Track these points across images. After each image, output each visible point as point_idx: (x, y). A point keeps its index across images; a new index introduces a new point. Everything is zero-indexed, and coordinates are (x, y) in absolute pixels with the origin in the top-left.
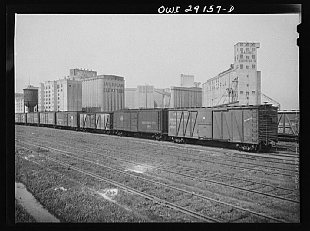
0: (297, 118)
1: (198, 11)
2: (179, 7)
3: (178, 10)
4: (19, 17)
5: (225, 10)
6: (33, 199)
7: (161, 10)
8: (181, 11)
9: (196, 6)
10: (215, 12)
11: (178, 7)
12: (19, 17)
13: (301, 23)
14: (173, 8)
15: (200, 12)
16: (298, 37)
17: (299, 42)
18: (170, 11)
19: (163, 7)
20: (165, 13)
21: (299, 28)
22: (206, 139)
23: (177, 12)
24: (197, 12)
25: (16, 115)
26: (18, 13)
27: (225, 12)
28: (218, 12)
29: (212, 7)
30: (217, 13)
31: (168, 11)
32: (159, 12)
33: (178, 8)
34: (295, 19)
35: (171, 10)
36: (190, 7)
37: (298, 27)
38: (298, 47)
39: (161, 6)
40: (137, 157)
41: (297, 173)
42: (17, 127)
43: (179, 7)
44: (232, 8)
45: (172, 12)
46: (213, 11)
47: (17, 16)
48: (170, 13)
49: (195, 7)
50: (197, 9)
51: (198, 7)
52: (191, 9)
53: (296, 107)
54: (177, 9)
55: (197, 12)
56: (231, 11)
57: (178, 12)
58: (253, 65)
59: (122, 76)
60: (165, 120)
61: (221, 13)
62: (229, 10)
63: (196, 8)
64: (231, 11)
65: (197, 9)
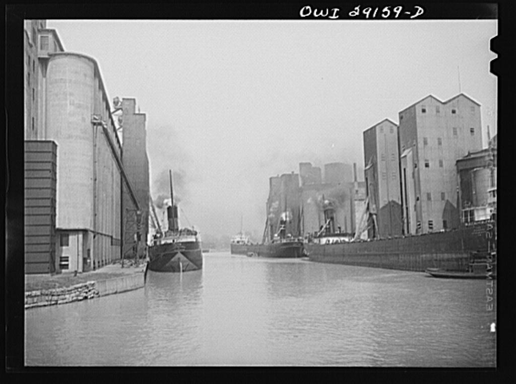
1: (369, 16)
2: (338, 10)
8: (343, 16)
9: (396, 7)
10: (392, 17)
11: (336, 10)
13: (497, 35)
17: (495, 67)
19: (308, 7)
21: (495, 45)
22: (479, 223)
24: (367, 17)
27: (408, 17)
28: (397, 16)
29: (389, 9)
32: (302, 15)
33: (337, 11)
34: (489, 28)
35: (324, 13)
38: (495, 78)
39: (307, 6)
42: (28, 277)
43: (338, 10)
44: (352, 14)
48: (320, 18)
49: (363, 9)
50: (398, 11)
51: (401, 8)
52: (334, 11)
55: (367, 17)
56: (417, 14)
58: (68, 257)
60: (417, 186)
61: (400, 18)
62: (415, 14)
63: (367, 11)
64: (417, 14)
65: (398, 11)
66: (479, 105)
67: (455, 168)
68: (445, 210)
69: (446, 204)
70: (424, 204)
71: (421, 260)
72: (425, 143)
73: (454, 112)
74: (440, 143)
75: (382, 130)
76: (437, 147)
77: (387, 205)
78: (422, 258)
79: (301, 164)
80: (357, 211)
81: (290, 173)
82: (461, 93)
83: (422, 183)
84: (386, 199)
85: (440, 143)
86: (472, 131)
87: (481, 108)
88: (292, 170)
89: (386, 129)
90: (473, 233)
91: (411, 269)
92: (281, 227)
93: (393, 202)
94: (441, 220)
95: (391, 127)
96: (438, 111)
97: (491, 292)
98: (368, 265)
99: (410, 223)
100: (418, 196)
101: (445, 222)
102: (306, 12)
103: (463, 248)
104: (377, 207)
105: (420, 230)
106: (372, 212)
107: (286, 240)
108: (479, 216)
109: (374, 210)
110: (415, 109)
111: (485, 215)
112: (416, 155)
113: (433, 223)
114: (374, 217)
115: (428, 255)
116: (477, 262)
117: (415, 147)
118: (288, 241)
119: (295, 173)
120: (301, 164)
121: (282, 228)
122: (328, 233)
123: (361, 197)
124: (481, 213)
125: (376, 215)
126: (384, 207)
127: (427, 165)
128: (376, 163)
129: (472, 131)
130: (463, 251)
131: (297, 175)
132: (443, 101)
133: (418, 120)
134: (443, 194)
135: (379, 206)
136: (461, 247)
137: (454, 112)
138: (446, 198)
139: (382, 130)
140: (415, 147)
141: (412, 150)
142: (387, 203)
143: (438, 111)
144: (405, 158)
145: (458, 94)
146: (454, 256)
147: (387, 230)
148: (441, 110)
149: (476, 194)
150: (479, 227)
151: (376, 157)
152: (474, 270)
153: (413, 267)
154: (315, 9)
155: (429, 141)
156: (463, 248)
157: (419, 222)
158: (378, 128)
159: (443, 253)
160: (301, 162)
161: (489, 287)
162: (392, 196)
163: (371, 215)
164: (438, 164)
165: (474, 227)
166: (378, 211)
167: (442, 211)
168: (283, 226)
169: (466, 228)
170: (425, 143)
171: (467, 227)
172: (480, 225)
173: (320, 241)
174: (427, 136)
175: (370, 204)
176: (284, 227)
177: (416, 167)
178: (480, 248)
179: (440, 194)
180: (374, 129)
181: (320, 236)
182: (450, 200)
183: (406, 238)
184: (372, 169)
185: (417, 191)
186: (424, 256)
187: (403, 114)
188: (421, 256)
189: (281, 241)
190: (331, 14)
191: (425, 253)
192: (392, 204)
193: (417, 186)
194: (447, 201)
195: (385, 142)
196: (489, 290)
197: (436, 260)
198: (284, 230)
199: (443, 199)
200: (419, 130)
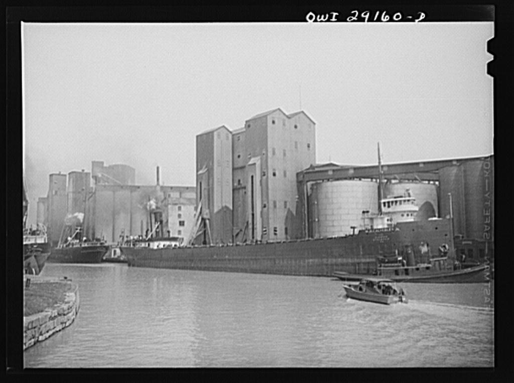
0: (491, 165)
2: (337, 14)
3: (336, 18)
4: (27, 29)
5: (410, 17)
6: (129, 269)
7: (311, 17)
11: (335, 14)
12: (27, 29)
14: (327, 16)
15: (371, 20)
16: (492, 36)
17: (492, 69)
18: (322, 19)
19: (311, 13)
20: (316, 21)
21: (492, 46)
23: (334, 19)
24: (366, 20)
25: (494, 19)
26: (25, 21)
30: (347, 21)
31: (320, 18)
33: (336, 16)
34: (485, 30)
35: (325, 18)
36: (355, 13)
37: (489, 43)
40: (178, 294)
41: (488, 286)
43: (337, 14)
45: (324, 20)
46: (401, 19)
47: (25, 26)
48: (321, 21)
53: (487, 150)
54: (334, 16)
57: (356, 19)
59: (101, 160)
63: (365, 14)
66: (314, 124)
67: (295, 179)
68: (287, 217)
69: (288, 212)
70: (271, 211)
71: (306, 264)
72: (274, 153)
73: (296, 127)
74: (285, 154)
75: (219, 135)
76: (282, 158)
77: (220, 210)
78: (308, 263)
79: (93, 162)
80: (171, 215)
81: (80, 171)
82: (302, 110)
83: (270, 192)
84: (220, 205)
85: (285, 154)
86: (309, 146)
87: (316, 126)
88: (83, 168)
89: (223, 136)
90: (374, 240)
91: (301, 274)
92: (77, 229)
93: (226, 207)
94: (284, 227)
95: (227, 134)
96: (284, 125)
97: (488, 293)
98: (229, 270)
99: (256, 229)
100: (265, 203)
101: (286, 229)
102: (398, 17)
103: (361, 253)
104: (211, 213)
105: (266, 236)
106: (205, 216)
107: (88, 244)
108: (377, 225)
109: (207, 214)
110: (267, 119)
111: (383, 224)
112: (265, 163)
113: (278, 229)
114: (207, 222)
115: (316, 260)
116: (385, 266)
117: (264, 156)
118: (90, 245)
119: (86, 171)
120: (93, 162)
121: (78, 231)
122: (158, 238)
123: (175, 201)
124: (380, 221)
125: (209, 219)
126: (219, 212)
127: (274, 175)
128: (212, 169)
129: (309, 146)
130: (361, 256)
131: (87, 174)
132: (287, 114)
133: (269, 129)
134: (285, 202)
135: (213, 210)
136: (359, 252)
137: (296, 127)
138: (288, 207)
139: (219, 135)
140: (264, 156)
141: (261, 159)
142: (220, 208)
143: (284, 125)
144: (253, 166)
145: (299, 111)
146: (350, 261)
147: (219, 235)
148: (286, 123)
149: (318, 204)
150: (382, 234)
151: (213, 163)
152: (382, 274)
153: (295, 272)
154: (338, 13)
155: (276, 151)
156: (361, 253)
157: (265, 228)
158: (215, 133)
159: (336, 257)
160: (93, 160)
161: (487, 290)
162: (225, 202)
163: (203, 219)
164: (282, 173)
165: (376, 234)
166: (211, 216)
167: (285, 218)
168: (79, 228)
169: (366, 235)
170: (274, 153)
171: (367, 234)
172: (382, 232)
173: (149, 245)
174: (275, 147)
175: (203, 209)
176: (80, 230)
177: (264, 175)
178: (386, 253)
179: (283, 203)
180: (211, 134)
181: (151, 240)
182: (291, 209)
183: (247, 247)
184: (207, 174)
185: (264, 199)
186: (311, 260)
187: (251, 124)
188: (306, 261)
189: (81, 245)
190: (331, 17)
191: (311, 258)
192: (225, 210)
193: (264, 193)
194: (289, 209)
195: (221, 151)
196: (487, 290)
197: (327, 265)
198: (80, 233)
199: (285, 207)
200: (269, 140)
